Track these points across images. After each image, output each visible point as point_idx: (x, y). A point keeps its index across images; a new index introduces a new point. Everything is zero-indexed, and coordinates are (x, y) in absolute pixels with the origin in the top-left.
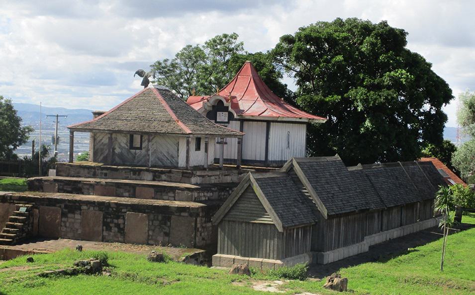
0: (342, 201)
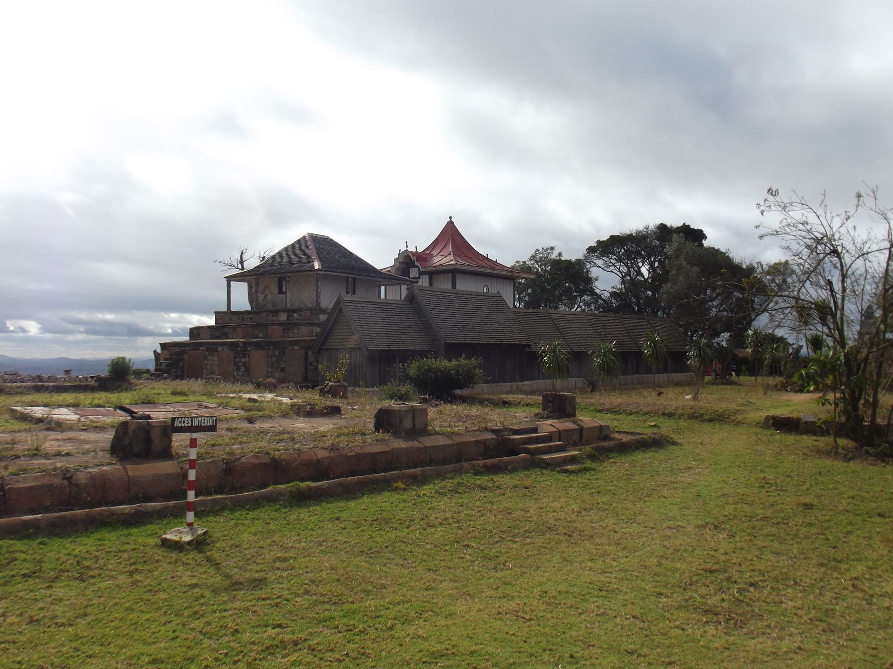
0: (479, 332)
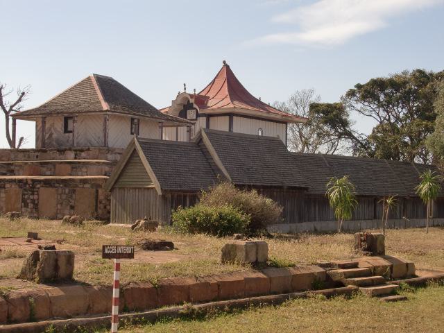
0: (262, 174)
